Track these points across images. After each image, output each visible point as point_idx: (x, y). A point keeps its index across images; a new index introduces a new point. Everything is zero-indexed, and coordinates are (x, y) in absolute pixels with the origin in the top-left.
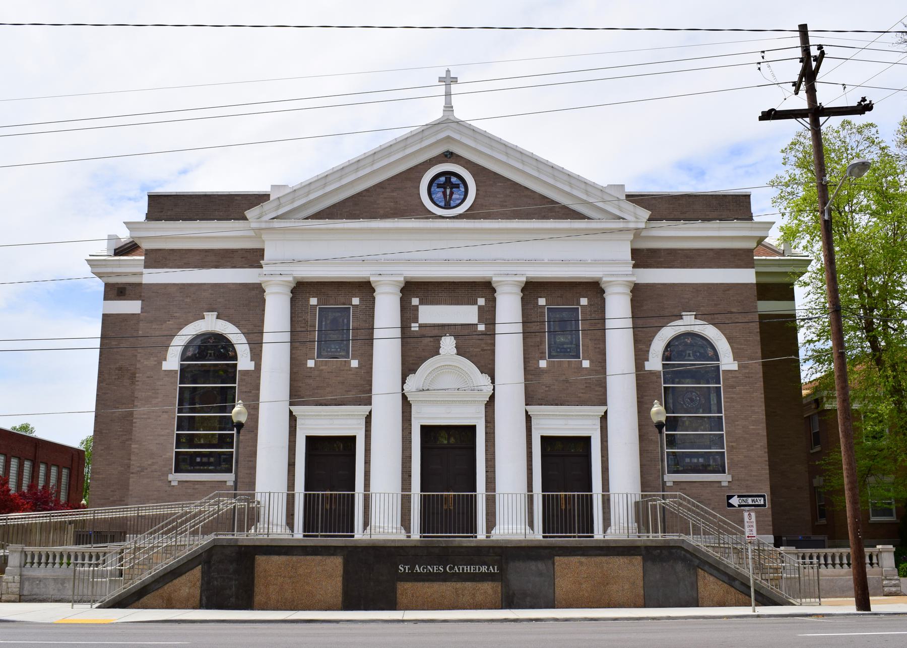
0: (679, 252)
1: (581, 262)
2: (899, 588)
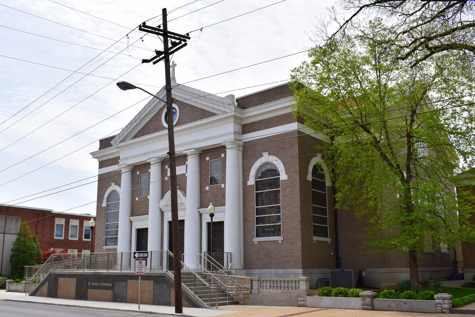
0: (263, 121)
1: (214, 137)
2: (305, 302)
